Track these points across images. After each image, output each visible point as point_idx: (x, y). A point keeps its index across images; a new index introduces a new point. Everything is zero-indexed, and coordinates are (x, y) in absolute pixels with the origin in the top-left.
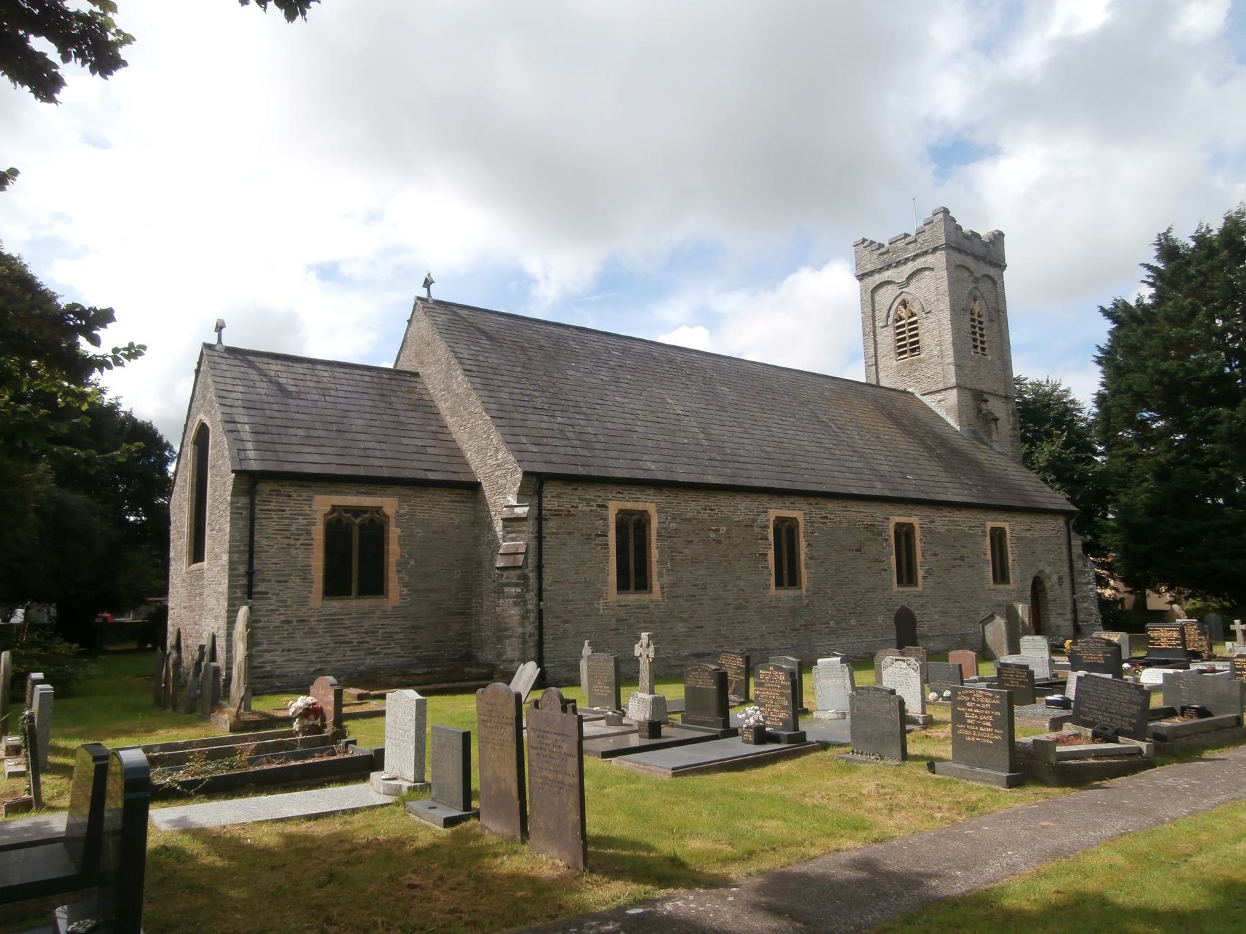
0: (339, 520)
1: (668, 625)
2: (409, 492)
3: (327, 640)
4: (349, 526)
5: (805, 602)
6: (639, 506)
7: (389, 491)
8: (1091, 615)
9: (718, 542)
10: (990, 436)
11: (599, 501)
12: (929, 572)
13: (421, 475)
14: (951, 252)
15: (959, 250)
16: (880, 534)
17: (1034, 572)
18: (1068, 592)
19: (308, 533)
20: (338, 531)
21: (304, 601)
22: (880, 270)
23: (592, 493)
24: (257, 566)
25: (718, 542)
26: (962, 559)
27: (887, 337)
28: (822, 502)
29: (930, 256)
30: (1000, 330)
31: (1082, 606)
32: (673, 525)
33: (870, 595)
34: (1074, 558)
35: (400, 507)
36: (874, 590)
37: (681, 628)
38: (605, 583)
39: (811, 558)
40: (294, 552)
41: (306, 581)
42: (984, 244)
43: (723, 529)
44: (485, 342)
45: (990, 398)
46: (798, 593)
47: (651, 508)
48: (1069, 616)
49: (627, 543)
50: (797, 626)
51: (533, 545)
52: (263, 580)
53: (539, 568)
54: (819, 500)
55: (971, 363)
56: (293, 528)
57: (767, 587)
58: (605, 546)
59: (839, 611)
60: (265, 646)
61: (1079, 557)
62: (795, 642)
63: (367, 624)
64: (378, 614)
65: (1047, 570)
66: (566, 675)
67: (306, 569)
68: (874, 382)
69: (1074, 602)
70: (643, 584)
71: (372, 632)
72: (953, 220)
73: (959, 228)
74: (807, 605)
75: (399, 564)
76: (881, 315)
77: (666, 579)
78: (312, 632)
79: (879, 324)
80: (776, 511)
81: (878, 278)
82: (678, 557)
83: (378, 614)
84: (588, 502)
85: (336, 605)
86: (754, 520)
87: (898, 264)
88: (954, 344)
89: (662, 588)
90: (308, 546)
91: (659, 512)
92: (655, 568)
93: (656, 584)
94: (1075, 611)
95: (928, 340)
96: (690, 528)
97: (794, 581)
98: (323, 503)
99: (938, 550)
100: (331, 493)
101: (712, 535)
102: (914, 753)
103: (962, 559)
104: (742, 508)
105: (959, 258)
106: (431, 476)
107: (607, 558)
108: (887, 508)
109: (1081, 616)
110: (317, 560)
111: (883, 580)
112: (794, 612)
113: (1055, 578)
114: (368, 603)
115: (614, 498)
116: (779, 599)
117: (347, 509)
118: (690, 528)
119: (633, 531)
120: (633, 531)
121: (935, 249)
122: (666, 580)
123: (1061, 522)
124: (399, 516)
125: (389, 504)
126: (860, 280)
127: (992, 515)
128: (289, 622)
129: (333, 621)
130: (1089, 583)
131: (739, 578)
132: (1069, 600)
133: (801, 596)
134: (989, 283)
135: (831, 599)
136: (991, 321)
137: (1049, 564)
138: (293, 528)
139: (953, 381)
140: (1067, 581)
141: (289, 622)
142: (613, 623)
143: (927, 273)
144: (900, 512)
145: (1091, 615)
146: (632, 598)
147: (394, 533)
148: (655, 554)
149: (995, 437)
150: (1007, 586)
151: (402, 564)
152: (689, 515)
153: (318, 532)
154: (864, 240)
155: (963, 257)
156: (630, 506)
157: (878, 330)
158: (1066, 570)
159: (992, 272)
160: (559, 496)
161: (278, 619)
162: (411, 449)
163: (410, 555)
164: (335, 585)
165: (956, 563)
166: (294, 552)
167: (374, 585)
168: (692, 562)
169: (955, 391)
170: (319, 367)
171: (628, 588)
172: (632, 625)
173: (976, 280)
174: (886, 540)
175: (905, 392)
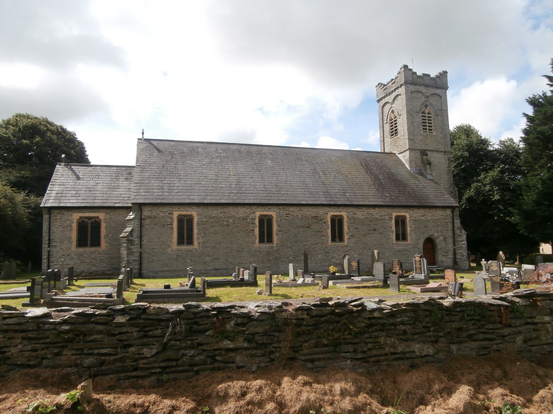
0: (83, 222)
1: (202, 258)
2: (109, 211)
3: (78, 261)
4: (87, 223)
5: (275, 249)
6: (188, 213)
7: (102, 211)
8: (463, 256)
9: (229, 226)
10: (426, 171)
11: (169, 212)
12: (352, 236)
13: (112, 205)
14: (409, 85)
15: (413, 83)
16: (322, 220)
17: (426, 236)
18: (451, 246)
19: (71, 226)
20: (82, 226)
21: (69, 248)
22: (384, 97)
23: (166, 209)
24: (52, 237)
25: (229, 226)
26: (375, 230)
27: (387, 127)
28: (287, 208)
29: (400, 89)
30: (443, 120)
31: (458, 251)
32: (205, 220)
33: (314, 246)
34: (456, 229)
35: (106, 216)
36: (317, 244)
37: (208, 259)
38: (171, 242)
39: (279, 231)
40: (66, 232)
41: (70, 242)
42: (433, 79)
43: (231, 221)
44: (156, 153)
45: (428, 153)
46: (271, 245)
47: (194, 214)
48: (452, 256)
49: (335, 231)
50: (270, 259)
51: (137, 229)
52: (55, 242)
53: (141, 237)
54: (285, 207)
55: (420, 137)
56: (65, 224)
57: (254, 243)
58: (172, 228)
59: (295, 253)
60: (55, 263)
61: (458, 228)
62: (269, 265)
63: (93, 256)
64: (97, 253)
65: (436, 235)
66: (152, 275)
67: (70, 238)
68: (382, 151)
69: (455, 250)
70: (190, 242)
71: (95, 259)
72: (411, 70)
73: (415, 73)
74: (277, 250)
75: (105, 236)
76: (385, 118)
77: (201, 240)
78: (72, 259)
79: (385, 122)
80: (395, 213)
81: (384, 101)
82: (207, 232)
83: (97, 253)
84: (164, 212)
85: (81, 250)
86: (248, 217)
87: (390, 94)
88: (408, 129)
89: (199, 243)
90: (71, 230)
91: (198, 215)
92: (195, 236)
93: (196, 242)
94: (455, 254)
95: (400, 128)
96: (214, 220)
97: (270, 240)
98: (76, 216)
99: (358, 227)
100: (79, 212)
101: (225, 223)
102: (211, 296)
103: (375, 230)
104: (242, 212)
105: (413, 88)
106: (116, 205)
107: (172, 233)
108: (326, 209)
109: (458, 256)
110: (74, 235)
111: (322, 240)
112: (269, 253)
113: (441, 238)
114: (93, 249)
115: (177, 211)
116: (260, 248)
117: (86, 218)
118: (214, 220)
119: (337, 223)
120: (337, 223)
121: (401, 85)
122: (201, 240)
123: (449, 212)
124: (105, 219)
125: (101, 215)
126: (378, 102)
127: (396, 210)
128: (64, 255)
129: (80, 255)
130: (462, 241)
131: (239, 240)
132: (452, 250)
133: (273, 247)
134: (437, 97)
135: (290, 248)
136: (437, 115)
137: (438, 232)
138: (65, 224)
139: (408, 147)
140: (450, 241)
141: (64, 255)
142: (175, 257)
143: (400, 97)
144: (334, 210)
145: (463, 256)
146: (184, 247)
147: (103, 225)
148: (195, 231)
149: (429, 172)
150: (406, 242)
151: (106, 236)
152: (213, 215)
153: (75, 226)
154: (379, 84)
155: (417, 87)
156: (184, 213)
157: (384, 125)
158: (450, 234)
159: (438, 91)
160: (151, 211)
161: (60, 254)
162: (115, 195)
163: (110, 233)
164: (81, 243)
165: (370, 232)
166: (66, 232)
167: (96, 243)
168: (214, 233)
169: (408, 152)
170: (97, 168)
171: (184, 244)
172: (184, 257)
173: (427, 97)
174: (325, 223)
175: (391, 153)
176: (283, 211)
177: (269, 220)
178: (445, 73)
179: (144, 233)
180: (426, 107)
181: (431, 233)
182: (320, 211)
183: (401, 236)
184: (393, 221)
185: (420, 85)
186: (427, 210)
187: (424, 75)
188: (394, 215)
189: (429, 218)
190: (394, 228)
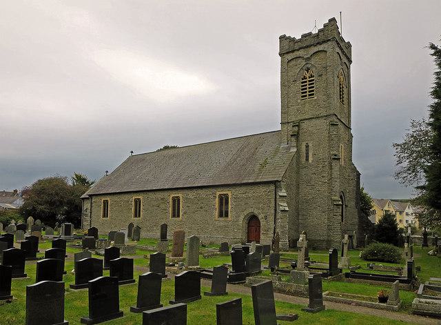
6: (225, 193)
12: (185, 213)
26: (201, 208)
47: (180, 195)
80: (219, 192)
103: (201, 208)
127: (219, 189)
134: (322, 55)
137: (259, 209)
173: (308, 59)
175: (174, 147)
176: (146, 195)
177: (226, 196)
178: (333, 20)
179: (93, 210)
180: (308, 70)
181: (250, 210)
182: (166, 194)
183: (223, 213)
184: (217, 199)
185: (298, 50)
186: (249, 187)
187: (304, 36)
188: (218, 193)
189: (250, 195)
190: (217, 206)
